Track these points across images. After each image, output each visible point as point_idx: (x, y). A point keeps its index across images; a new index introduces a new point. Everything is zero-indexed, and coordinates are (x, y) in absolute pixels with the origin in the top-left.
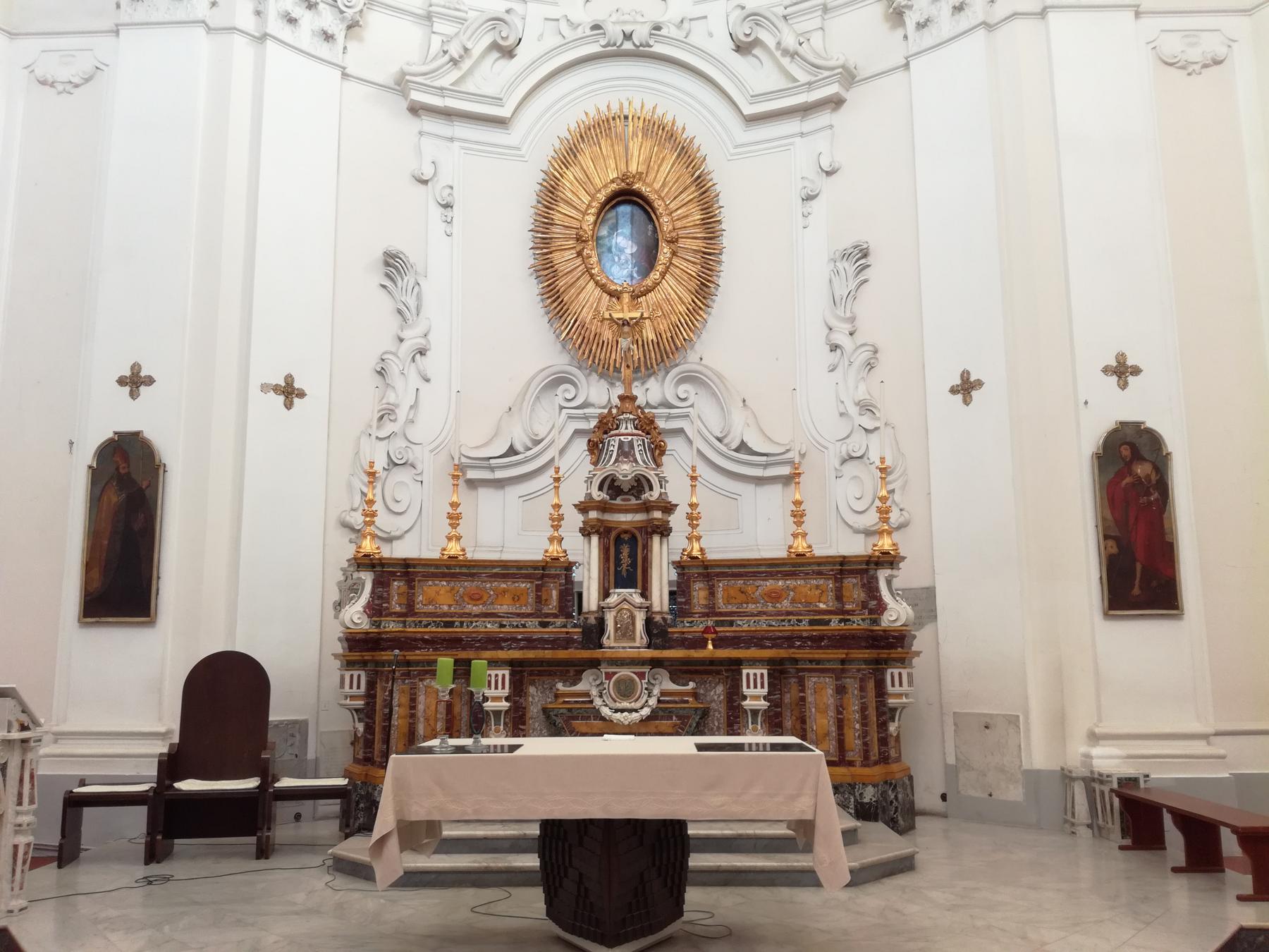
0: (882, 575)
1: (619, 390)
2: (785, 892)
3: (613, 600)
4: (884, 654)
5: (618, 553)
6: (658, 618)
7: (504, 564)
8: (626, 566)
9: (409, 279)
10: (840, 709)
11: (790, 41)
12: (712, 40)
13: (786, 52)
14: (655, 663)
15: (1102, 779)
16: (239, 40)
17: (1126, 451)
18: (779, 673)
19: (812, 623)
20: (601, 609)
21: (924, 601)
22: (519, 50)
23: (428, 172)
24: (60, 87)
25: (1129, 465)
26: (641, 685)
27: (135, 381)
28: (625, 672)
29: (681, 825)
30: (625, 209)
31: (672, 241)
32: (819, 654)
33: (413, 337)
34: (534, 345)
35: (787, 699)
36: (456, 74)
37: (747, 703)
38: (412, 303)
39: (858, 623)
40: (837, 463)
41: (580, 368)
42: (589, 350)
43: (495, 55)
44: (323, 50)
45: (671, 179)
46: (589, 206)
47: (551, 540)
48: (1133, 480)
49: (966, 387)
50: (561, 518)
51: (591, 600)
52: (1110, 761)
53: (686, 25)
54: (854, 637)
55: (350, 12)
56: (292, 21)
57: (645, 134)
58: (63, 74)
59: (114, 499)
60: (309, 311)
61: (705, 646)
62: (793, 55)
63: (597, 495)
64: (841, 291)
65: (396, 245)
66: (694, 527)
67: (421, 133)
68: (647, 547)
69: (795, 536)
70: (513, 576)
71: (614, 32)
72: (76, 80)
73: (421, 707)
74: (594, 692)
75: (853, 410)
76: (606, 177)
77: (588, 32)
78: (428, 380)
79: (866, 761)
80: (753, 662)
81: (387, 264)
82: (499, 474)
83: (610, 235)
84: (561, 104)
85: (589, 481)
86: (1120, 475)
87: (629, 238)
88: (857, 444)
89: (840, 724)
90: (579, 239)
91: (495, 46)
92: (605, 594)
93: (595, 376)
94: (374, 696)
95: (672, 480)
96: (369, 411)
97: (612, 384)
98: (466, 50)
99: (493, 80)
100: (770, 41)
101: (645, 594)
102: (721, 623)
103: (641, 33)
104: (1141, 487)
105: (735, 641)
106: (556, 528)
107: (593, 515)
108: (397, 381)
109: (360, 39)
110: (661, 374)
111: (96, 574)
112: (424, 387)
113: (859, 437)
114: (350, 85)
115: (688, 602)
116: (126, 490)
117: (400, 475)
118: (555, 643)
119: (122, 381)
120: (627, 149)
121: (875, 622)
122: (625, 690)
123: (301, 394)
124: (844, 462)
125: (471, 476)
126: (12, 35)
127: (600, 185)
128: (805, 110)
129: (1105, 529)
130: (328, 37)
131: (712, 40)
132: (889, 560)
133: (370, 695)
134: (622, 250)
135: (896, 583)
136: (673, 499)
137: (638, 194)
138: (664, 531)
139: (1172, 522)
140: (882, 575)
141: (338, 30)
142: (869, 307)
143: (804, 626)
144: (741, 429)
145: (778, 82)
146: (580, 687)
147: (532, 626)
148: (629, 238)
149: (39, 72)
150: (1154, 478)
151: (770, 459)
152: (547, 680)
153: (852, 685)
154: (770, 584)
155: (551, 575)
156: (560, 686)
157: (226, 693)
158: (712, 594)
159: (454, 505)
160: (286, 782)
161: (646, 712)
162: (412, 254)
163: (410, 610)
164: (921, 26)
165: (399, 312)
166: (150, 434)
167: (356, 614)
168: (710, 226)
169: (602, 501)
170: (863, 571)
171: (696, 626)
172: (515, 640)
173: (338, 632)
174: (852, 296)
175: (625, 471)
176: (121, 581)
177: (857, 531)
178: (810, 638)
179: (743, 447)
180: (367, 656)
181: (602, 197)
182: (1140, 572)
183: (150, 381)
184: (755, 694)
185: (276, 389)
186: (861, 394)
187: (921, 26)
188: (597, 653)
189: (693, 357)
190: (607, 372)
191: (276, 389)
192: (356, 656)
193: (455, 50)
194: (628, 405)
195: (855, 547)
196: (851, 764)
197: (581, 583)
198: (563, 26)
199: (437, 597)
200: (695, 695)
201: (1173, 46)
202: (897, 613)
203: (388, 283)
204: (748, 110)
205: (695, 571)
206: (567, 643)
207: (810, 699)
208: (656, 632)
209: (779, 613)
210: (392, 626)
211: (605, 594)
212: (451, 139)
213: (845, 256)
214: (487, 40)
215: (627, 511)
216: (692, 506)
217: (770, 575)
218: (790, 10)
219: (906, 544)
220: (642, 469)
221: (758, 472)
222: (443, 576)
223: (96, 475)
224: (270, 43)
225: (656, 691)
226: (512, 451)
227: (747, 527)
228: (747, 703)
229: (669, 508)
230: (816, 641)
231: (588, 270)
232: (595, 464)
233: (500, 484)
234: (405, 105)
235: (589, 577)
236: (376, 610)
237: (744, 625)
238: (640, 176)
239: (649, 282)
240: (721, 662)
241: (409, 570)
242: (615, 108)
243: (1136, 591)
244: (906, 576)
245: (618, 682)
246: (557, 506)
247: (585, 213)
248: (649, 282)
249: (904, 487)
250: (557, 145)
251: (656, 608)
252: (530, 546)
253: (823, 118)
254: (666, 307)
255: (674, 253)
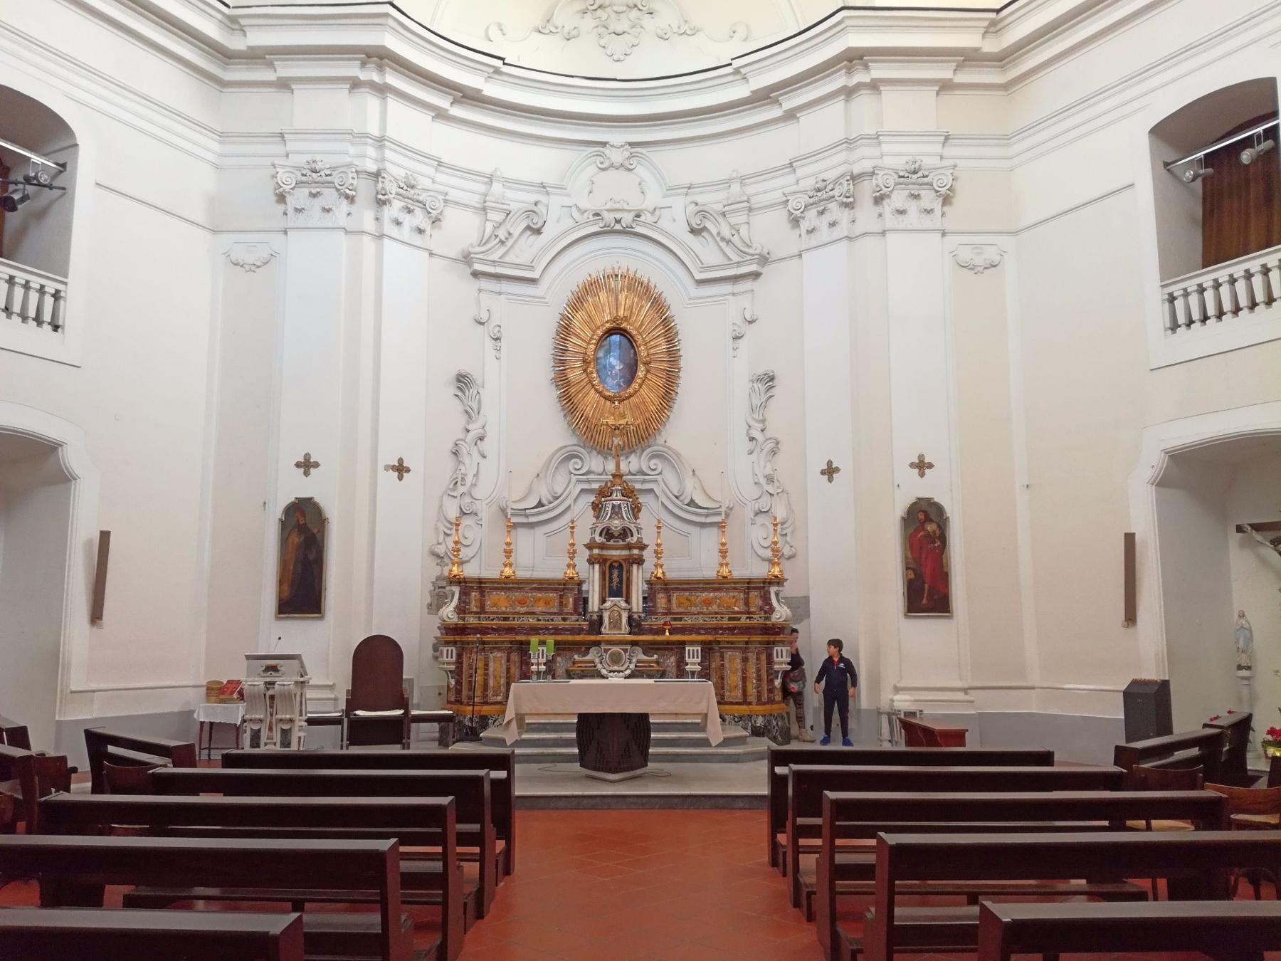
0: (773, 589)
1: (611, 467)
2: (702, 765)
3: (608, 604)
4: (772, 638)
5: (611, 574)
6: (636, 616)
7: (540, 582)
8: (616, 584)
9: (473, 391)
10: (744, 671)
11: (726, 232)
12: (674, 224)
13: (723, 239)
14: (634, 643)
15: (896, 713)
16: (366, 239)
17: (921, 516)
18: (708, 649)
19: (730, 619)
20: (601, 610)
21: (801, 606)
22: (543, 230)
23: (484, 317)
24: (248, 268)
25: (923, 524)
26: (625, 656)
27: (307, 465)
28: (616, 649)
29: (645, 717)
30: (616, 338)
31: (646, 364)
32: (732, 638)
33: (475, 428)
34: (553, 432)
35: (714, 665)
36: (503, 249)
37: (688, 668)
38: (475, 406)
39: (758, 620)
40: (752, 515)
41: (584, 447)
42: (592, 435)
43: (529, 233)
44: (417, 240)
45: (648, 319)
46: (591, 338)
47: (569, 566)
48: (925, 532)
49: (830, 471)
50: (575, 552)
51: (594, 604)
52: (903, 702)
53: (657, 212)
54: (753, 628)
55: (434, 213)
56: (398, 223)
57: (629, 290)
58: (250, 259)
59: (296, 540)
60: (411, 417)
61: (664, 633)
62: (728, 242)
63: (599, 539)
64: (757, 402)
65: (466, 369)
66: (659, 558)
67: (480, 291)
68: (629, 571)
69: (721, 565)
70: (545, 589)
71: (608, 217)
72: (258, 263)
73: (491, 669)
74: (597, 661)
75: (763, 481)
76: (605, 318)
77: (592, 218)
78: (485, 457)
79: (759, 702)
80: (692, 643)
81: (459, 381)
82: (532, 520)
83: (605, 356)
84: (667, 735)
85: (593, 530)
86: (917, 531)
87: (618, 367)
88: (765, 503)
89: (744, 680)
90: (584, 361)
91: (528, 228)
92: (603, 601)
93: (594, 453)
94: (462, 663)
95: (646, 527)
96: (446, 480)
97: (606, 458)
98: (510, 234)
99: (525, 251)
100: (714, 231)
101: (628, 601)
102: (675, 619)
103: (627, 218)
104: (930, 538)
105: (682, 630)
106: (572, 558)
107: (596, 551)
108: (466, 460)
109: (440, 228)
110: (639, 452)
111: (286, 587)
112: (483, 461)
113: (766, 498)
114: (436, 260)
115: (654, 606)
116: (304, 534)
117: (466, 521)
118: (573, 631)
119: (298, 465)
120: (617, 299)
121: (767, 619)
122: (616, 659)
123: (408, 470)
124: (756, 514)
125: (515, 521)
126: (214, 232)
127: (599, 323)
128: (736, 279)
129: (907, 563)
130: (420, 231)
131: (674, 224)
132: (778, 581)
133: (459, 662)
134: (613, 367)
135: (781, 595)
136: (645, 542)
137: (625, 330)
138: (640, 561)
139: (948, 559)
140: (773, 589)
141: (425, 225)
142: (773, 413)
143: (725, 621)
144: (691, 490)
145: (720, 260)
146: (588, 658)
147: (558, 620)
148: (618, 367)
149: (233, 257)
150: (938, 533)
151: (710, 512)
152: (568, 653)
153: (752, 657)
154: (705, 595)
155: (569, 588)
156: (576, 657)
157: (376, 661)
158: (669, 601)
159: (508, 544)
160: (414, 712)
161: (628, 672)
162: (476, 375)
163: (482, 609)
164: (810, 232)
165: (466, 412)
166: (318, 499)
167: (449, 612)
168: (673, 355)
169: (603, 543)
170: (762, 587)
171: (658, 621)
172: (547, 629)
173: (438, 622)
174: (764, 406)
175: (616, 524)
176: (302, 591)
177: (764, 560)
178: (728, 629)
179: (692, 503)
180: (458, 638)
181: (600, 332)
182: (927, 590)
183: (316, 465)
184: (693, 661)
185: (393, 468)
186: (768, 471)
187: (810, 232)
188: (599, 638)
189: (660, 440)
190: (604, 450)
191: (393, 468)
192: (450, 638)
193: (502, 234)
194: (617, 480)
195: (759, 570)
196: (750, 704)
197: (588, 592)
198: (574, 210)
199: (498, 602)
200: (657, 662)
201: (966, 255)
202: (781, 613)
203: (460, 394)
204: (699, 276)
205: (657, 587)
206: (579, 631)
207: (727, 665)
208: (635, 625)
209: (710, 613)
210: (472, 620)
211: (603, 601)
212: (500, 293)
213: (759, 380)
214: (523, 225)
215: (617, 549)
216: (658, 545)
217: (705, 590)
218: (727, 208)
219: (788, 570)
220: (626, 524)
221: (702, 520)
222: (502, 589)
223: (284, 524)
224: (386, 241)
225: (634, 660)
226: (540, 504)
227: (692, 556)
228: (688, 668)
229: (643, 547)
230: (731, 630)
231: (591, 382)
232: (597, 517)
233: (531, 526)
234: (469, 271)
235: (594, 590)
236: (461, 610)
237: (688, 621)
238: (626, 319)
239: (631, 390)
240: (673, 643)
241: (481, 585)
242: (609, 271)
243: (924, 601)
244: (788, 590)
245: (612, 655)
246: (573, 545)
247: (588, 343)
248: (631, 390)
249: (793, 532)
250: (570, 294)
251: (635, 610)
252: (554, 569)
253: (747, 285)
254: (642, 407)
255: (648, 371)
